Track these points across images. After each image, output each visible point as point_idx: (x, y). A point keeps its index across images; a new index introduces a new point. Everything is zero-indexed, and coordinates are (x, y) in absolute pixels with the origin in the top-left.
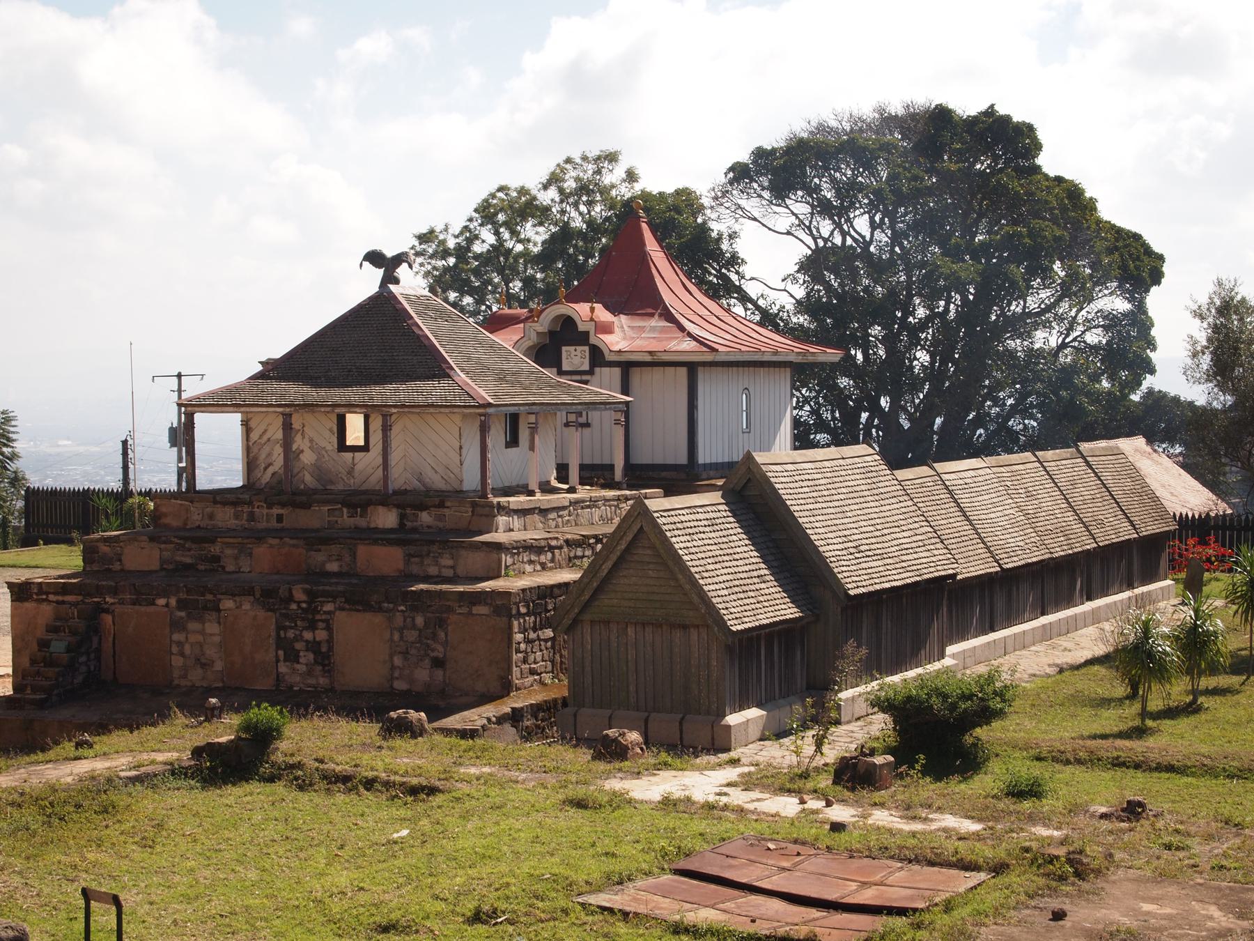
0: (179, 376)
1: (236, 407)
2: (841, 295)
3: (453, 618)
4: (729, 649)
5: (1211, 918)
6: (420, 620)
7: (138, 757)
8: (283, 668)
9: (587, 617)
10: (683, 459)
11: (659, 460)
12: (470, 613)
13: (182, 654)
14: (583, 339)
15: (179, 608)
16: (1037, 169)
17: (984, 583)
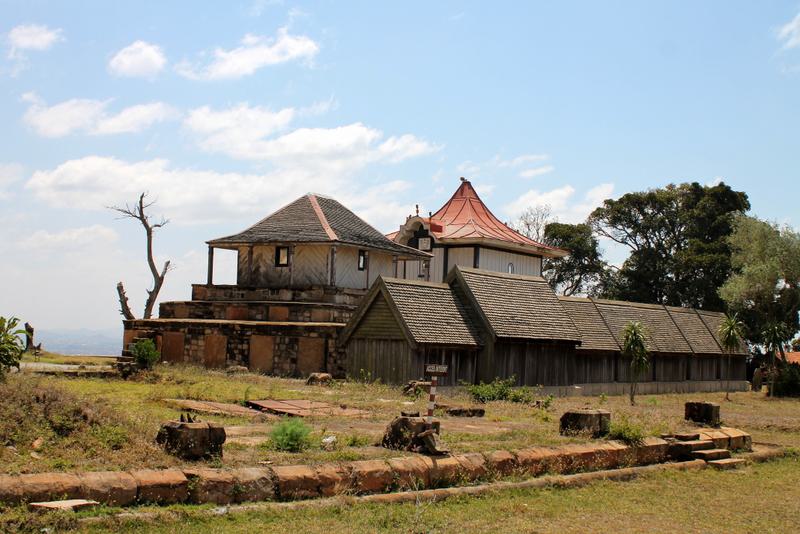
3: (301, 339)
6: (287, 340)
9: (355, 336)
12: (309, 337)
13: (188, 355)
15: (189, 333)
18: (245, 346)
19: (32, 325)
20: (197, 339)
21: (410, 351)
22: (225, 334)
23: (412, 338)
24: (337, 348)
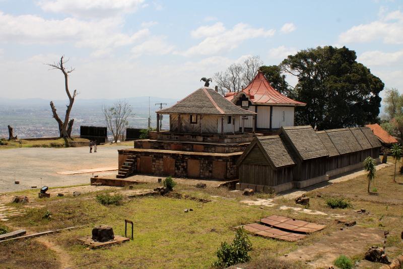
0: (161, 104)
1: (168, 113)
2: (307, 90)
4: (275, 171)
5: (376, 237)
6: (207, 162)
7: (27, 221)
8: (176, 171)
10: (269, 127)
11: (263, 127)
13: (155, 167)
14: (247, 99)
16: (356, 62)
17: (336, 158)
18: (185, 164)
19: (12, 127)
20: (159, 160)
21: (272, 171)
22: (174, 158)
23: (274, 165)
24: (230, 165)
